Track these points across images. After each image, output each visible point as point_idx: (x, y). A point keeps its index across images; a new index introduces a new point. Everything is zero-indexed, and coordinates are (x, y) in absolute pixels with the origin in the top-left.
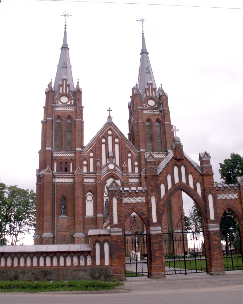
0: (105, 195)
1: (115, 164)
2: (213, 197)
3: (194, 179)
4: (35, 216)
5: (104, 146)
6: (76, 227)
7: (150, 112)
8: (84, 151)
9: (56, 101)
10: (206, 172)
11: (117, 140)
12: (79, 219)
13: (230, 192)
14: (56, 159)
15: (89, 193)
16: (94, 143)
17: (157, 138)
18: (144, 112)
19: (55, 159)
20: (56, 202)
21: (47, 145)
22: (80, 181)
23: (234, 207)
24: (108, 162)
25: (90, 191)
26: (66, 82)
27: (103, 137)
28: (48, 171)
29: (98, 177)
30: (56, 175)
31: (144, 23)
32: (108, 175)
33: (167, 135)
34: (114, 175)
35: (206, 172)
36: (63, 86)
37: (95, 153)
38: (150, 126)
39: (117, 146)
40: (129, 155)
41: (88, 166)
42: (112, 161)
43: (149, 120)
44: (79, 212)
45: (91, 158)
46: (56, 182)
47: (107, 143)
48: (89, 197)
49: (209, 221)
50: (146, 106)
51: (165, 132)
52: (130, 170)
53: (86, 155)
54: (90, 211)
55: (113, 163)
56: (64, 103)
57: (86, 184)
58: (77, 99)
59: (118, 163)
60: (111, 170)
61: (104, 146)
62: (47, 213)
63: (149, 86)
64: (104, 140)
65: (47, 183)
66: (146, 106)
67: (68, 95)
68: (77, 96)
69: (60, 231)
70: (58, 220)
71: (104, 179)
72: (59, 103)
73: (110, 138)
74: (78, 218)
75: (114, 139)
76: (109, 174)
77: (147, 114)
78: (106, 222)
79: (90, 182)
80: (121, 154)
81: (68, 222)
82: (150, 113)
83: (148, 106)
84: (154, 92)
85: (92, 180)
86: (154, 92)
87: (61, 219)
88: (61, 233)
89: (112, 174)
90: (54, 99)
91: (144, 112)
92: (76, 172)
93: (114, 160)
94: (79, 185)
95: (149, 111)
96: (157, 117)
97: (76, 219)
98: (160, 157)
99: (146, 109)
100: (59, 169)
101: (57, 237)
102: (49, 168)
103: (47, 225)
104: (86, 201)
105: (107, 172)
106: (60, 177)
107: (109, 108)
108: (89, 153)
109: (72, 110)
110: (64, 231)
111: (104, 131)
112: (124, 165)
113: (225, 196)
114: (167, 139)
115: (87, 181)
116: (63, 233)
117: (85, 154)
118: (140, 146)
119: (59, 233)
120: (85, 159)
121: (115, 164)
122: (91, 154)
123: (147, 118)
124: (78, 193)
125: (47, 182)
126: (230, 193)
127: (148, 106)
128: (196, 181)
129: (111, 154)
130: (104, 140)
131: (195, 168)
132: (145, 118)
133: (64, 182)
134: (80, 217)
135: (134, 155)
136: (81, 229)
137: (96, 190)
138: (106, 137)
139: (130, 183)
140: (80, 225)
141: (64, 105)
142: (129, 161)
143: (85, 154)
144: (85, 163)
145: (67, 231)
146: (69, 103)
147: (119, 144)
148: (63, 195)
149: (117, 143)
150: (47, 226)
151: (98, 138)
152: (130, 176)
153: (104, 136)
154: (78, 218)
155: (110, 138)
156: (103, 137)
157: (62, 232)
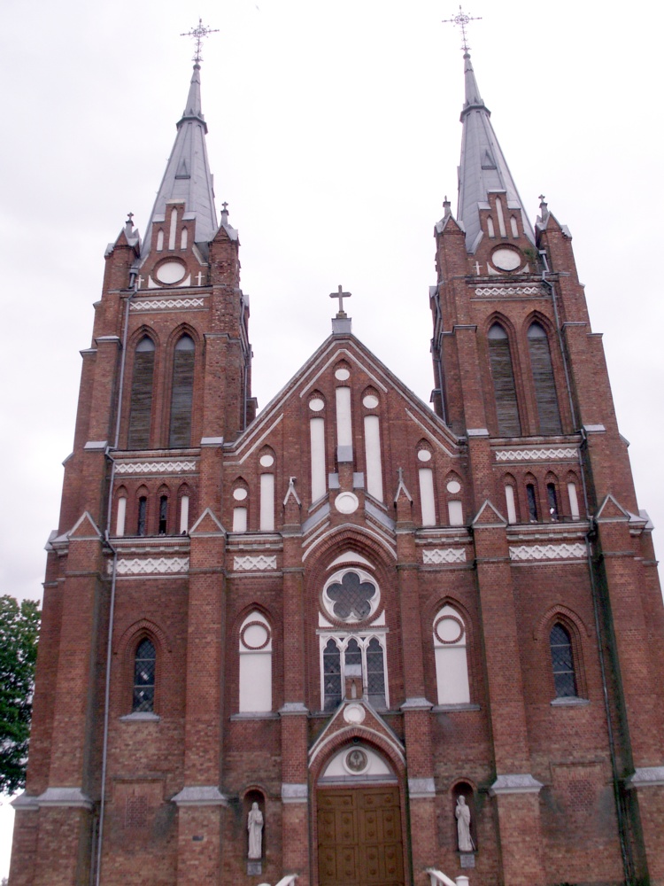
0: (323, 623)
1: (362, 494)
5: (317, 429)
7: (501, 292)
8: (237, 448)
11: (370, 402)
12: (201, 726)
15: (256, 616)
16: (275, 417)
20: (114, 653)
26: (180, 215)
27: (316, 391)
30: (116, 546)
32: (331, 537)
33: (575, 368)
34: (359, 538)
39: (372, 426)
41: (252, 506)
47: (329, 416)
51: (568, 359)
52: (428, 516)
55: (354, 490)
57: (240, 579)
59: (376, 489)
60: (347, 517)
61: (317, 429)
65: (75, 576)
66: (484, 269)
67: (183, 257)
69: (124, 782)
71: (318, 554)
73: (343, 398)
74: (198, 721)
76: (339, 533)
77: (490, 300)
78: (322, 740)
80: (387, 455)
81: (157, 740)
82: (503, 293)
87: (132, 728)
89: (349, 535)
91: (479, 292)
93: (358, 477)
94: (209, 580)
96: (530, 309)
99: (484, 282)
103: (64, 753)
104: (242, 649)
105: (330, 526)
107: (340, 287)
108: (256, 457)
110: (140, 781)
114: (580, 386)
116: (137, 789)
117: (241, 462)
120: (240, 478)
121: (362, 494)
122: (267, 461)
125: (77, 573)
129: (345, 455)
134: (206, 717)
135: (443, 454)
136: (208, 769)
141: (167, 289)
143: (241, 462)
144: (240, 494)
145: (154, 781)
149: (371, 413)
150: (66, 759)
154: (198, 721)
155: (343, 398)
157: (130, 782)
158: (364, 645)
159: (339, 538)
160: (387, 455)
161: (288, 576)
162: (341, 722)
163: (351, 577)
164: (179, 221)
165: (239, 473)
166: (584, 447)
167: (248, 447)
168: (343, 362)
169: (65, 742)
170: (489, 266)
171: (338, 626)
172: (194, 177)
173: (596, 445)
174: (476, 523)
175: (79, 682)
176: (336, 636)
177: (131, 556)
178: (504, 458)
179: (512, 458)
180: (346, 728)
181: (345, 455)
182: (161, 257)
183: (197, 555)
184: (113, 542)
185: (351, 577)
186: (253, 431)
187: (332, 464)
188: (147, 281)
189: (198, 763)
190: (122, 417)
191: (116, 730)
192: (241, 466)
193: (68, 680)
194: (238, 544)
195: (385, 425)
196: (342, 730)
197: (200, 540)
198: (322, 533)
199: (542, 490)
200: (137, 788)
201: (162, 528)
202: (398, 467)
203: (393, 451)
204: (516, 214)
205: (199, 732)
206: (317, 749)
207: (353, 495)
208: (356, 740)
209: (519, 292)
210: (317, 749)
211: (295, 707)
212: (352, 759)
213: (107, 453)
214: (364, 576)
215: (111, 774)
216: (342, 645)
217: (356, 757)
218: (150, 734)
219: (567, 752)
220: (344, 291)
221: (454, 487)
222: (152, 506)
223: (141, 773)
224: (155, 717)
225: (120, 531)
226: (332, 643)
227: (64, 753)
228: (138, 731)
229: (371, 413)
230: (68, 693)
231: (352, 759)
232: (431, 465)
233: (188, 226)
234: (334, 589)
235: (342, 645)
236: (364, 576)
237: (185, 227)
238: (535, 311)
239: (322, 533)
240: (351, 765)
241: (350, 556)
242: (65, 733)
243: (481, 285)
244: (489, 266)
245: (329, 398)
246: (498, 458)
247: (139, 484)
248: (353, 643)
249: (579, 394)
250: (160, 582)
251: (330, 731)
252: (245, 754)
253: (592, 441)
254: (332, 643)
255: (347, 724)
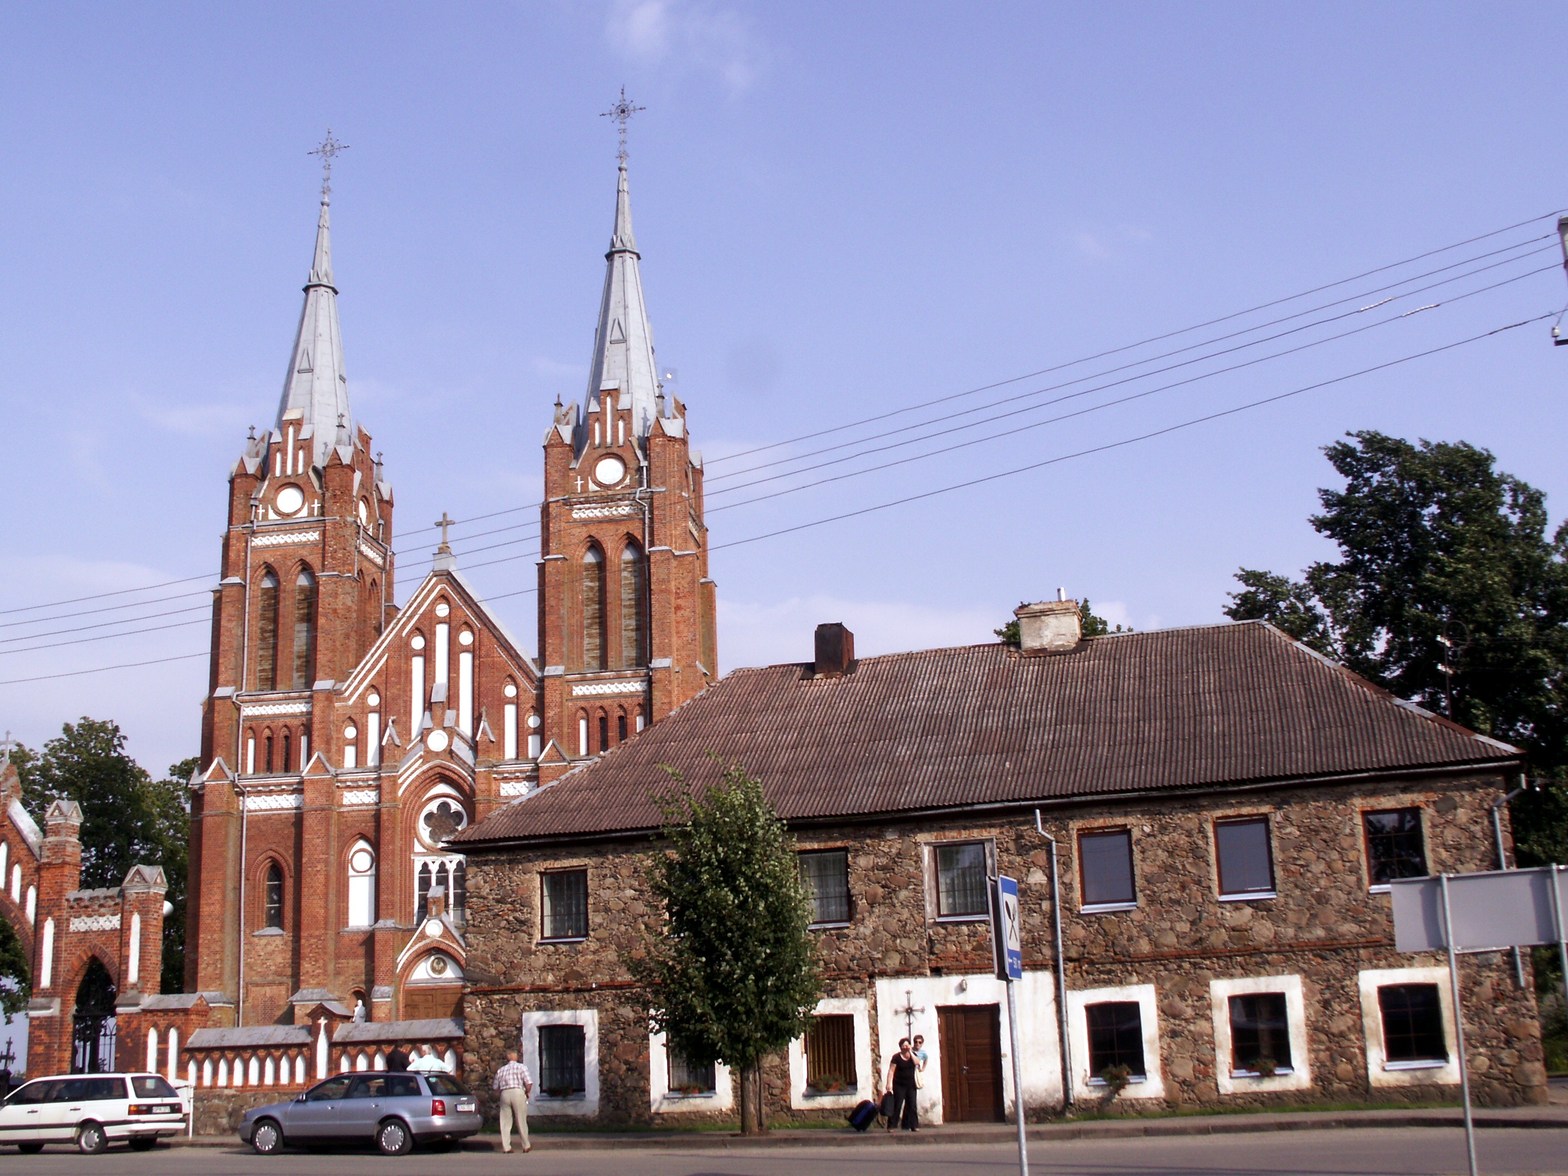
0: (418, 848)
1: (452, 732)
2: (55, 927)
3: (23, 877)
4: (1508, 802)
5: (417, 664)
6: (303, 970)
7: (597, 513)
8: (346, 690)
9: (261, 511)
10: (48, 857)
11: (466, 638)
12: (313, 941)
13: (102, 910)
14: (254, 726)
15: (362, 844)
16: (381, 657)
17: (625, 611)
18: (575, 516)
19: (248, 724)
20: (247, 879)
21: (222, 678)
22: (321, 801)
23: (106, 954)
24: (428, 724)
25: (363, 837)
26: (297, 432)
27: (418, 629)
28: (220, 773)
29: (386, 785)
30: (245, 786)
31: (633, 121)
32: (424, 772)
34: (447, 773)
35: (48, 857)
36: (286, 450)
37: (383, 695)
38: (601, 566)
39: (466, 660)
40: (510, 691)
41: (360, 743)
42: (443, 720)
43: (595, 545)
44: (315, 916)
45: (371, 712)
46: (249, 811)
47: (428, 654)
48: (361, 857)
49: (35, 991)
50: (584, 486)
52: (510, 750)
53: (355, 706)
54: (359, 914)
55: (444, 729)
56: (288, 515)
57: (348, 812)
58: (328, 495)
59: (466, 727)
60: (437, 754)
61: (417, 664)
62: (209, 921)
63: (605, 404)
64: (418, 643)
65: (211, 816)
67: (301, 483)
68: (330, 484)
69: (257, 985)
70: (251, 944)
71: (413, 788)
72: (272, 516)
73: (442, 631)
74: (311, 936)
75: (453, 634)
76: (431, 768)
77: (586, 522)
79: (361, 805)
80: (476, 692)
81: (283, 951)
82: (599, 515)
83: (592, 487)
84: (621, 424)
85: (369, 797)
86: (621, 424)
87: (264, 941)
88: (261, 990)
89: (439, 770)
90: (252, 502)
91: (576, 515)
92: (309, 772)
93: (450, 714)
94: (319, 816)
95: (595, 508)
96: (623, 529)
97: (303, 941)
98: (625, 690)
99: (581, 503)
100: (266, 765)
101: (247, 1004)
102: (222, 762)
103: (208, 965)
104: (351, 872)
105: (423, 763)
106: (260, 791)
107: (445, 515)
108: (363, 697)
109: (314, 536)
110: (270, 984)
111: (419, 606)
112: (484, 732)
113: (89, 923)
115: (355, 801)
116: (268, 991)
117: (351, 702)
118: (547, 653)
119: (254, 989)
120: (350, 718)
121: (452, 732)
122: (373, 700)
123: (585, 535)
124: (313, 846)
125: (213, 813)
126: (102, 915)
127: (592, 487)
128: (26, 881)
129: (439, 695)
130: (418, 643)
131: (29, 849)
132: (582, 533)
133: (276, 809)
134: (317, 933)
136: (319, 975)
137: (377, 831)
138: (425, 630)
139: (506, 797)
140: (316, 961)
141: (288, 523)
142: (510, 711)
143: (351, 702)
144: (350, 732)
145: (281, 984)
146: (304, 513)
147: (474, 650)
148: (272, 853)
149: (465, 649)
150: (210, 969)
151: (396, 635)
152: (502, 773)
153: (421, 626)
154: (311, 936)
155: (442, 631)
156: (418, 630)
157: (263, 985)
158: (451, 867)
159: (431, 773)
160: (476, 692)
161: (384, 810)
162: (423, 936)
163: (444, 806)
164: (296, 440)
165: (349, 713)
166: (650, 682)
167: (356, 689)
168: (444, 597)
169: (208, 955)
170: (590, 482)
171: (431, 851)
172: (317, 370)
173: (660, 680)
174: (541, 762)
175: (218, 906)
176: (429, 860)
177: (259, 793)
178: (580, 693)
179: (587, 693)
180: (428, 941)
181: (439, 695)
182: (281, 483)
183: (309, 794)
184: (241, 783)
185: (444, 806)
186: (359, 673)
187: (428, 705)
188: (267, 510)
189: (310, 970)
190: (249, 659)
191: (251, 944)
192: (351, 707)
193: (208, 904)
194: (345, 781)
195: (477, 662)
196: (424, 942)
197: (312, 782)
198: (416, 769)
199: (613, 723)
200: (268, 989)
201: (287, 769)
202: (486, 704)
203: (482, 689)
204: (626, 416)
205: (311, 945)
206: (403, 958)
207: (444, 734)
208: (437, 951)
209: (615, 513)
210: (403, 958)
211: (387, 923)
212: (435, 965)
213: (234, 700)
214: (455, 806)
215: (248, 979)
216: (434, 868)
217: (438, 964)
218: (277, 946)
219: (268, 944)
220: (448, 519)
221: (532, 722)
222: (279, 745)
223: (270, 978)
224: (281, 932)
225: (250, 769)
226: (425, 865)
227: (208, 965)
228: (268, 944)
229: (465, 649)
230: (210, 916)
231: (435, 965)
232: (516, 701)
233: (305, 445)
234: (429, 817)
235: (434, 868)
236: (455, 806)
237: (301, 448)
238: (628, 533)
239: (416, 769)
240: (434, 970)
241: (442, 788)
242: (209, 948)
243: (578, 506)
244: (590, 482)
245: (428, 636)
246: (574, 694)
247: (264, 725)
248: (442, 865)
249: (653, 626)
250: (283, 816)
251: (415, 943)
252: (351, 961)
253: (656, 676)
254: (425, 865)
255: (428, 937)
